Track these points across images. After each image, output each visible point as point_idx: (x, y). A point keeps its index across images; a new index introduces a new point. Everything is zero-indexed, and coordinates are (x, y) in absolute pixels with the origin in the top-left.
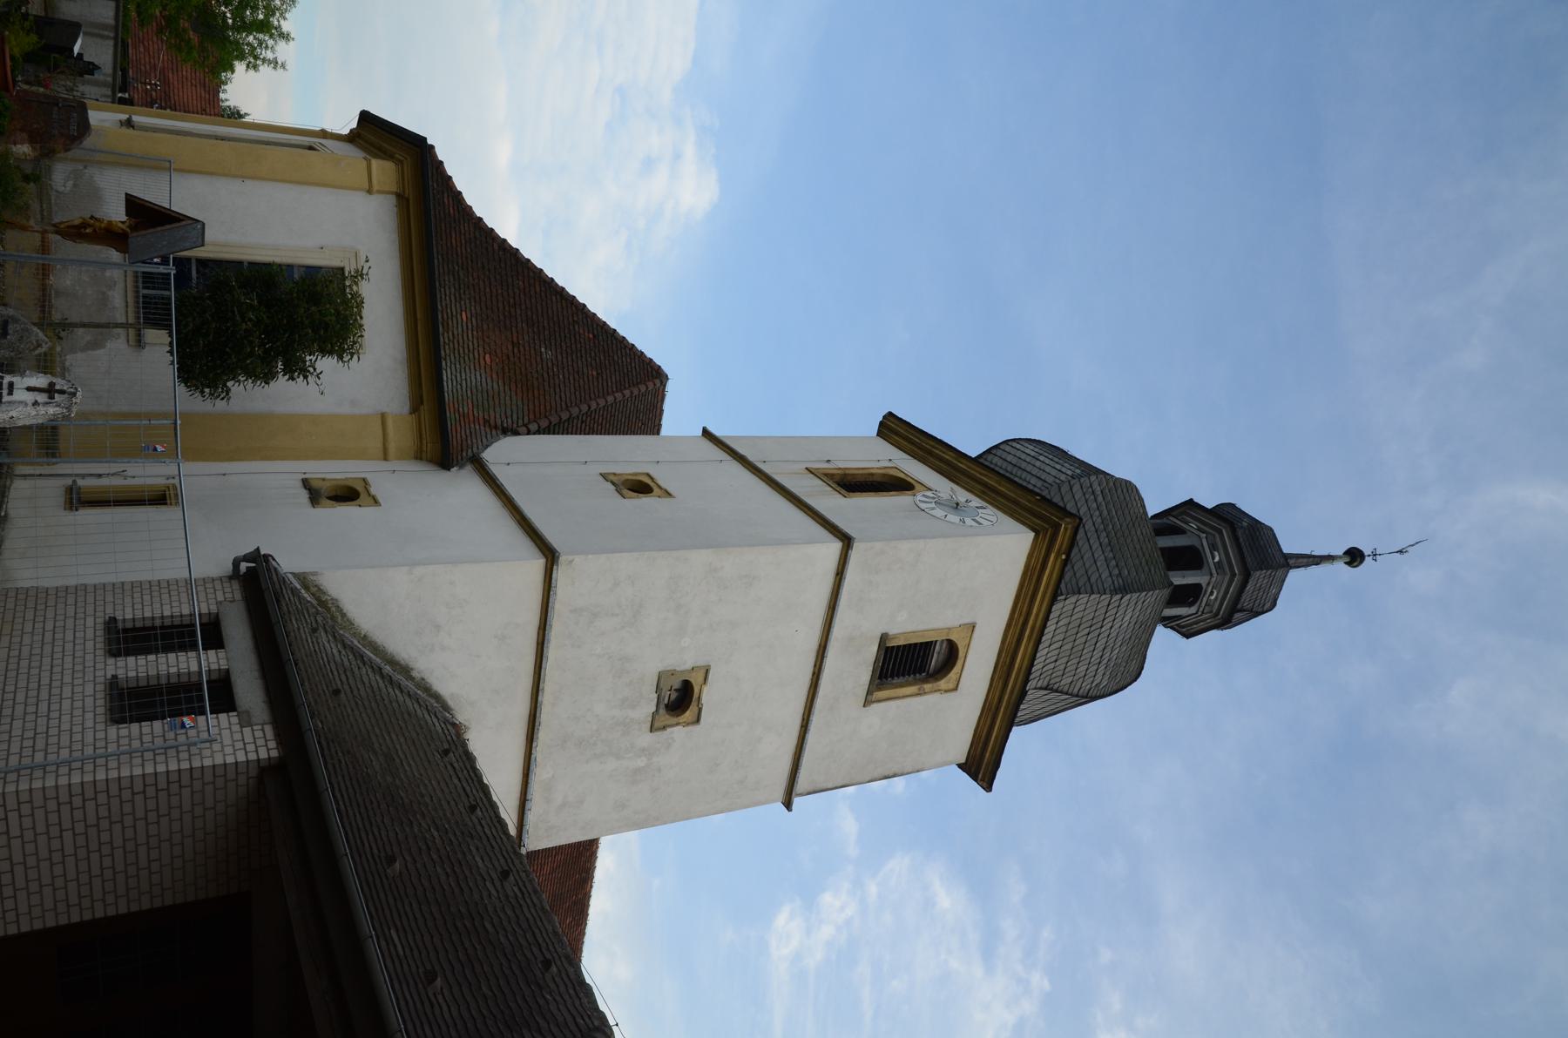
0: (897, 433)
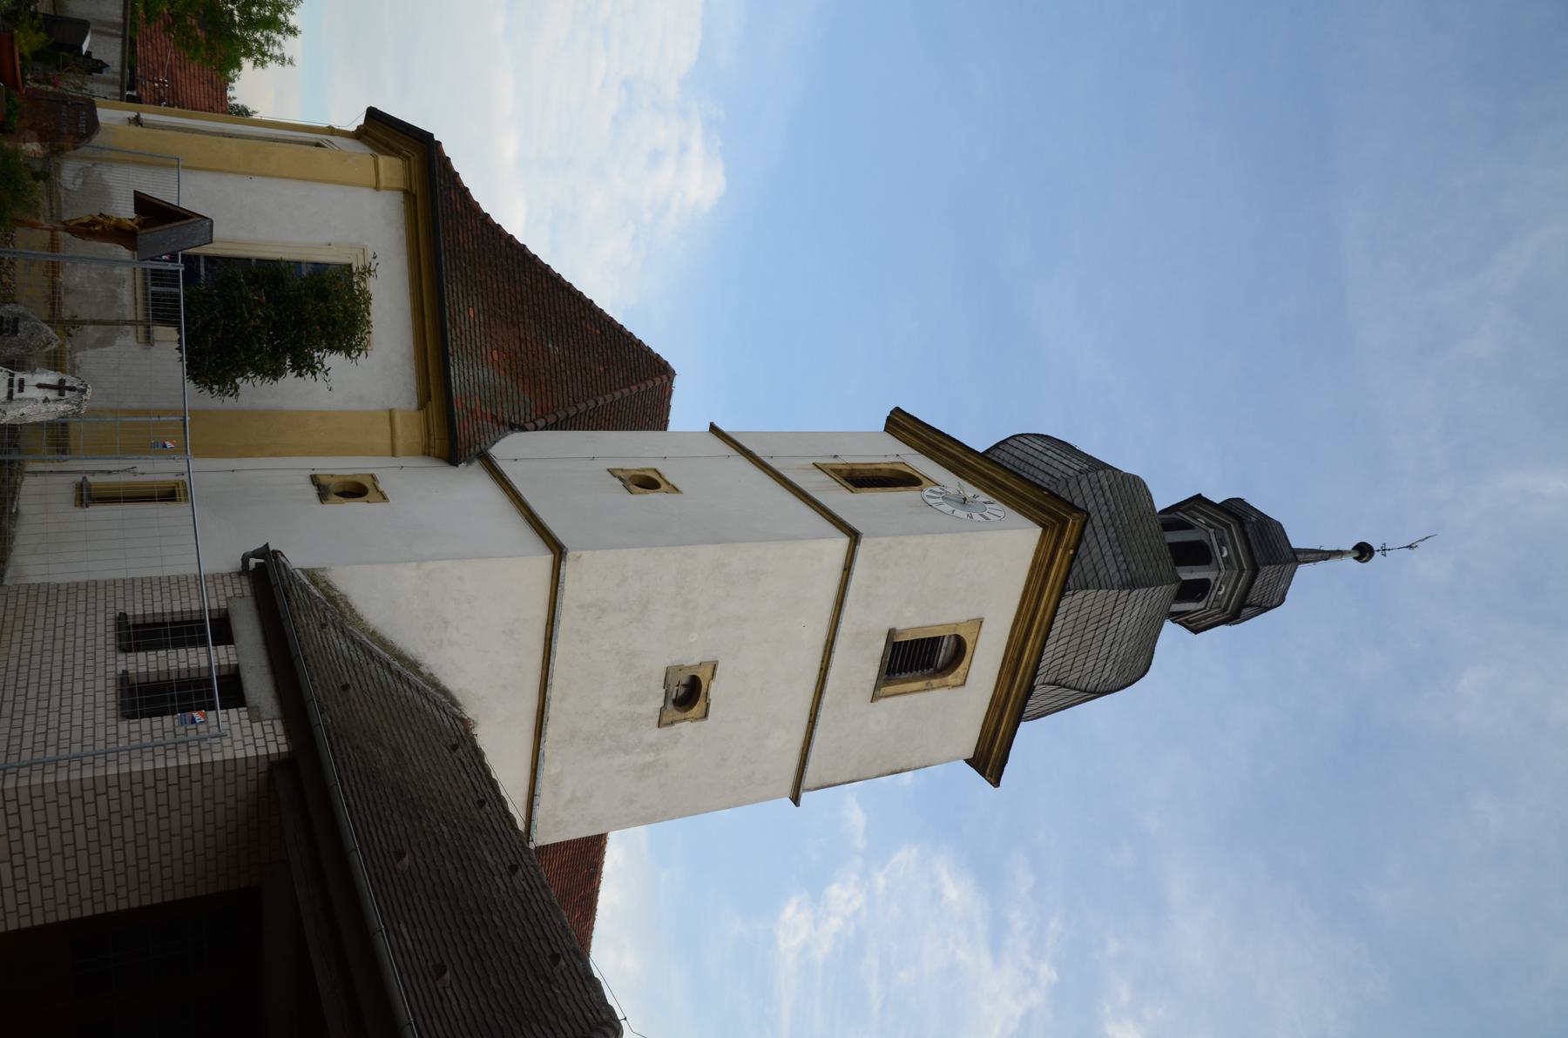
0: (905, 429)
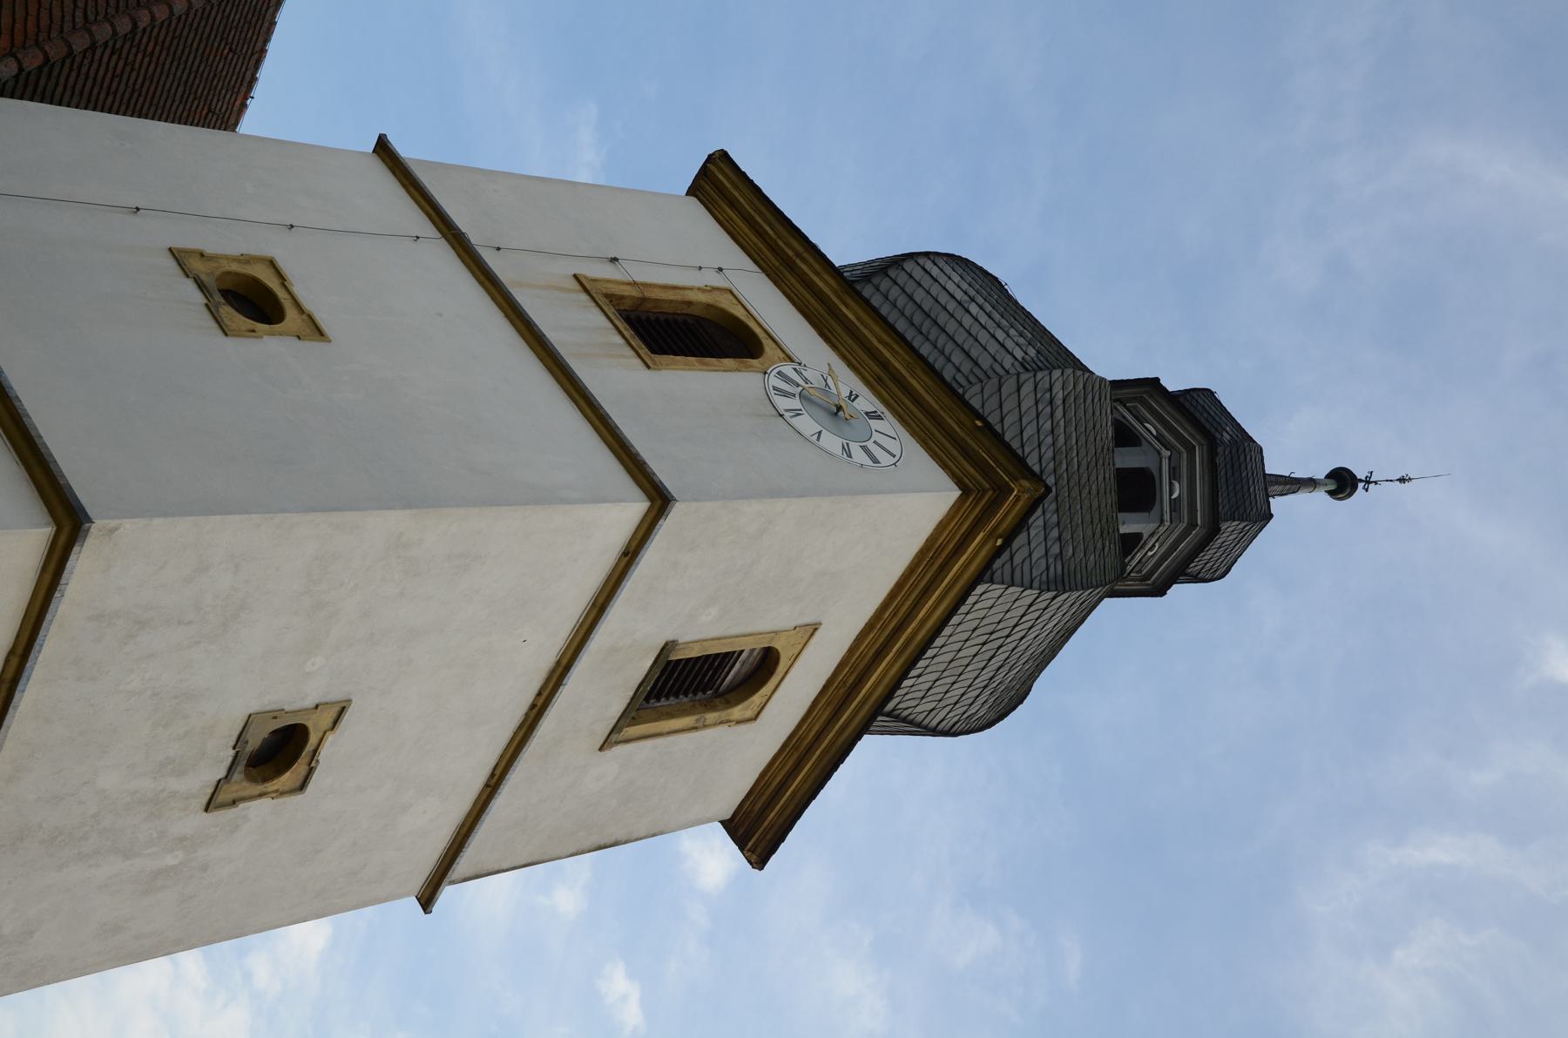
0: (733, 204)
